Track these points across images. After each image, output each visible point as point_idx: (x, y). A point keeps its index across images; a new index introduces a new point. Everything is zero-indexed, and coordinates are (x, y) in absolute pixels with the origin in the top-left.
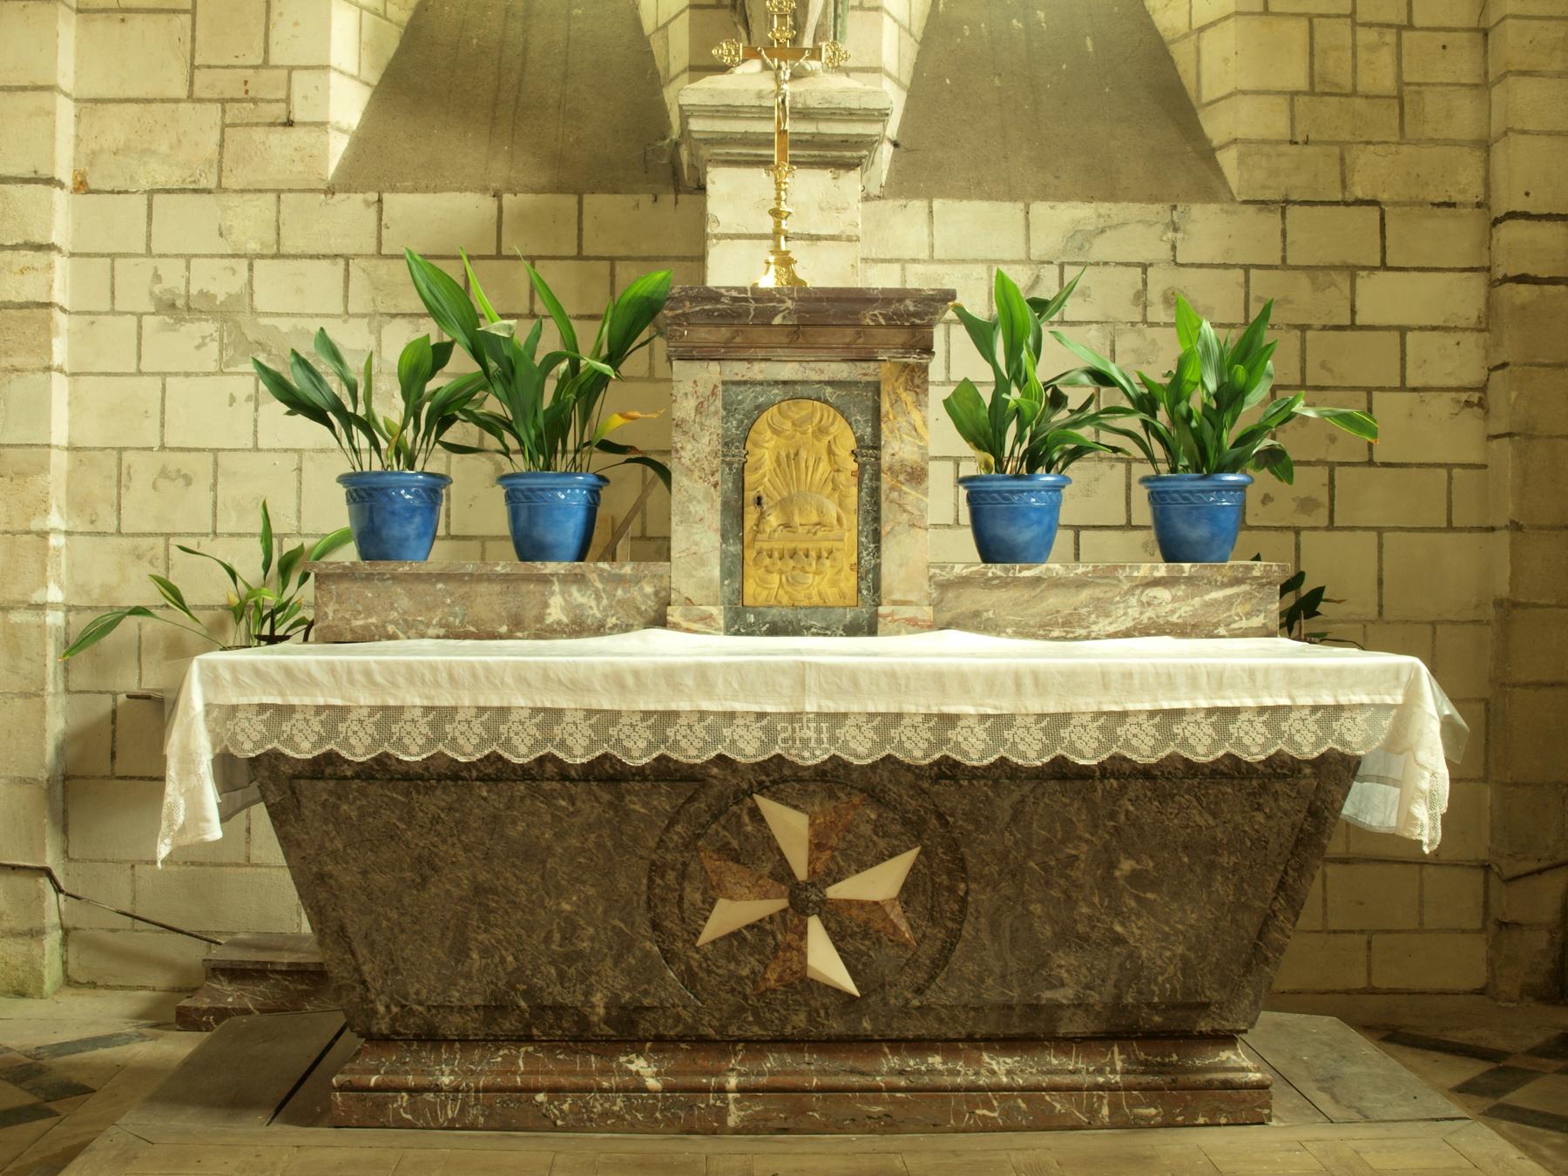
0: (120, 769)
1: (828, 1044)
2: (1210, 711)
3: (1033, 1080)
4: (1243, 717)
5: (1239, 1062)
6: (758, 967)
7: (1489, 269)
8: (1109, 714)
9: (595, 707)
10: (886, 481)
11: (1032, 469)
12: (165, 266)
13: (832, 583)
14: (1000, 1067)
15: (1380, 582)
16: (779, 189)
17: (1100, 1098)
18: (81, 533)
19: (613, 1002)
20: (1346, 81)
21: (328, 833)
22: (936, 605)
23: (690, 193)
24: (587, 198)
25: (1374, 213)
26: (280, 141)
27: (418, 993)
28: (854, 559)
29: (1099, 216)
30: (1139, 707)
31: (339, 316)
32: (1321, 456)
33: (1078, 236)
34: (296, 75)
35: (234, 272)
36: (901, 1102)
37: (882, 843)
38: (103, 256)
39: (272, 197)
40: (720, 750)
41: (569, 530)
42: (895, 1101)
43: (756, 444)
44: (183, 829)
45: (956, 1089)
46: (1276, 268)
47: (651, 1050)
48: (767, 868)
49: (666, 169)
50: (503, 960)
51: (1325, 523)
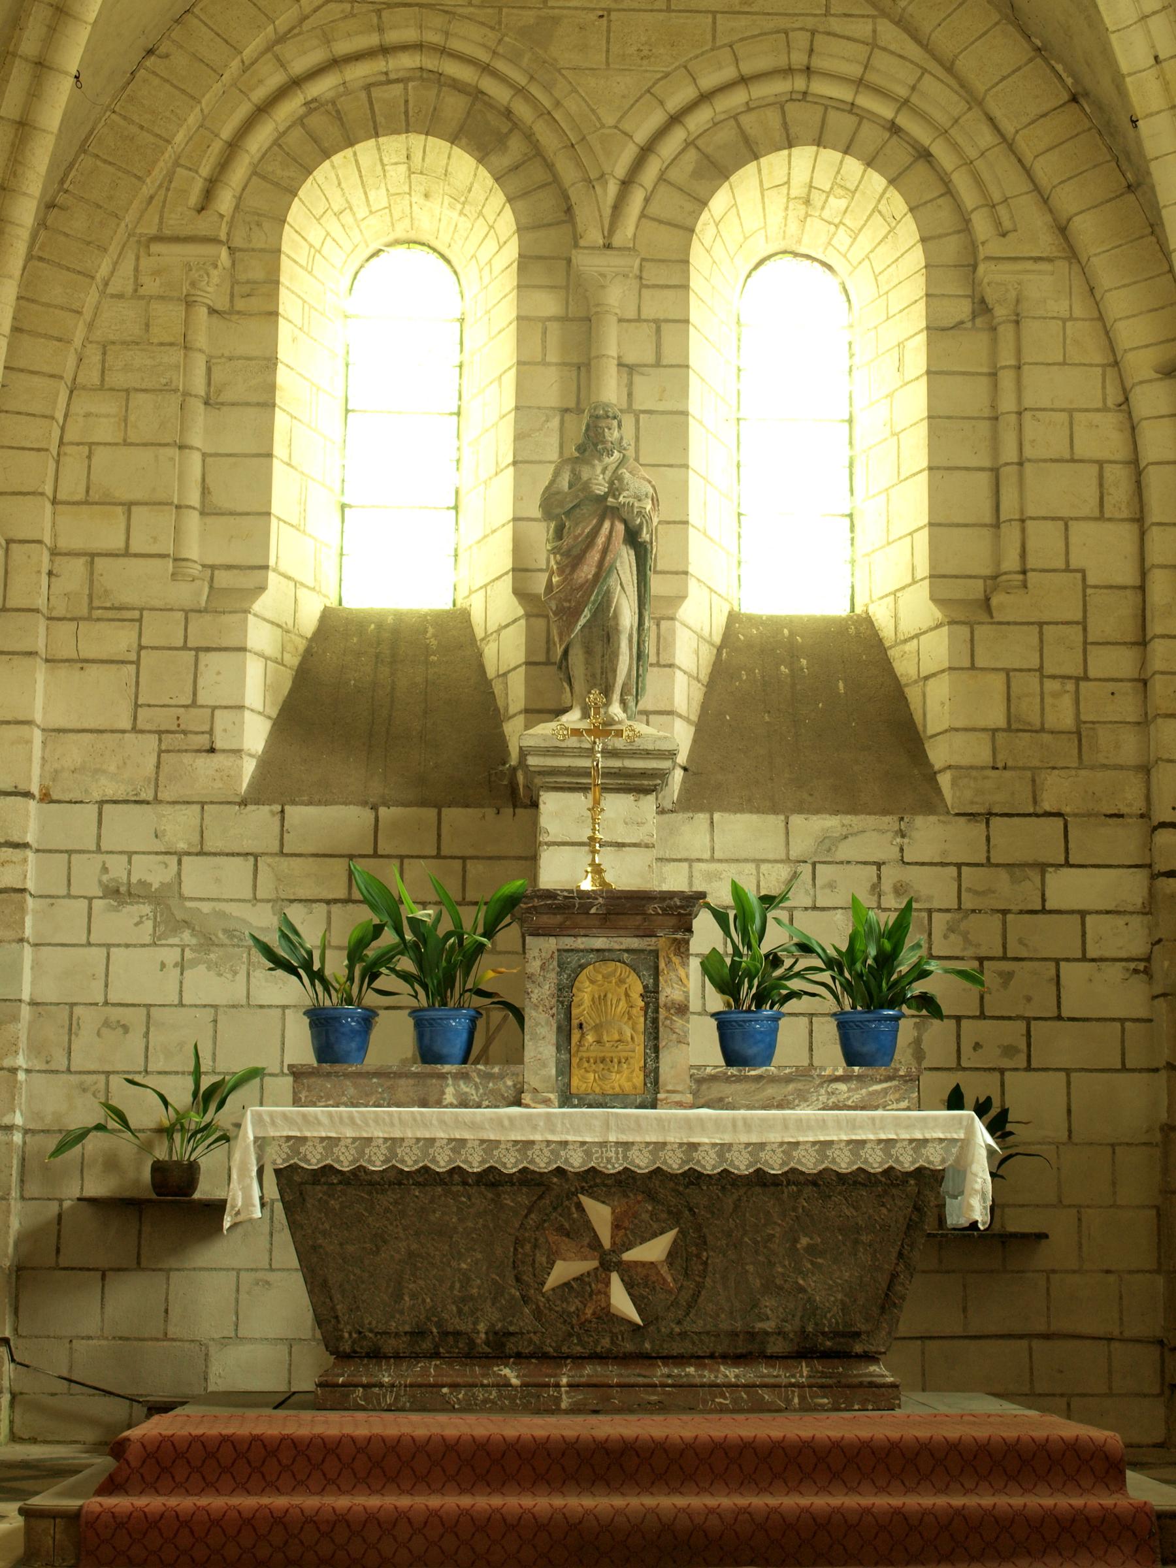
0: (63, 1262)
1: (625, 1359)
2: (849, 1142)
3: (751, 1381)
4: (868, 1145)
5: (879, 1371)
6: (580, 1306)
7: (1150, 866)
8: (789, 1143)
9: (486, 1138)
10: (663, 1013)
11: (759, 1006)
12: (111, 860)
13: (629, 1078)
14: (730, 1373)
15: (1069, 1111)
16: (594, 823)
17: (793, 1392)
18: (39, 1071)
19: (492, 1332)
20: (1036, 721)
21: (320, 1219)
22: (695, 1094)
23: (525, 807)
24: (445, 811)
25: (1059, 822)
26: (204, 765)
27: (370, 1323)
28: (642, 1064)
29: (843, 825)
30: (806, 1139)
31: (250, 901)
32: (1020, 1013)
33: (827, 841)
34: (217, 713)
35: (166, 866)
36: (669, 1394)
37: (655, 1226)
38: (61, 852)
39: (197, 808)
40: (559, 1164)
41: (457, 1046)
42: (664, 1393)
43: (579, 990)
44: (238, 1213)
45: (703, 1386)
46: (982, 865)
47: (514, 1363)
48: (586, 1241)
49: (511, 792)
50: (424, 1301)
51: (1024, 1065)
